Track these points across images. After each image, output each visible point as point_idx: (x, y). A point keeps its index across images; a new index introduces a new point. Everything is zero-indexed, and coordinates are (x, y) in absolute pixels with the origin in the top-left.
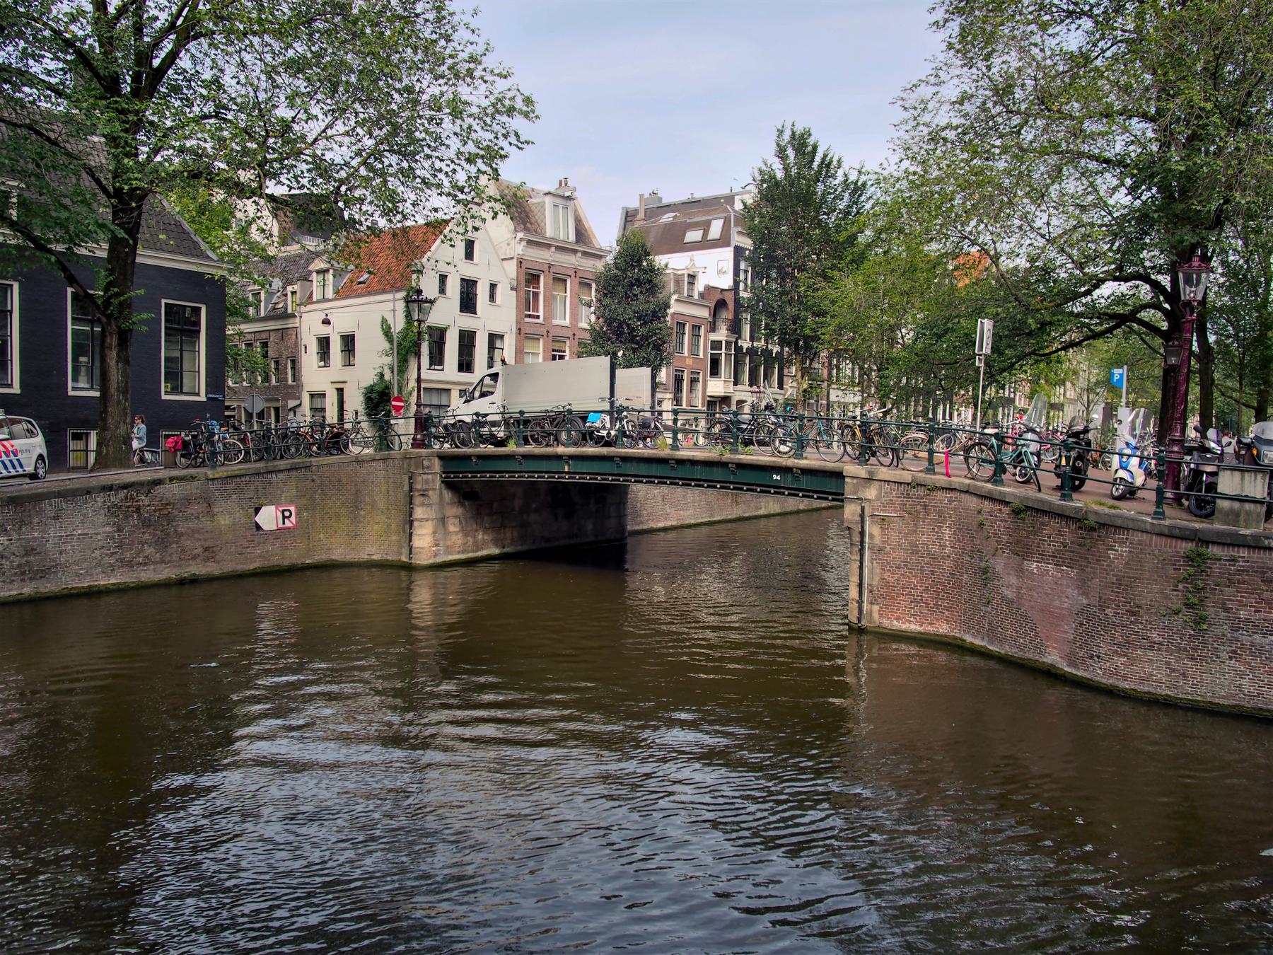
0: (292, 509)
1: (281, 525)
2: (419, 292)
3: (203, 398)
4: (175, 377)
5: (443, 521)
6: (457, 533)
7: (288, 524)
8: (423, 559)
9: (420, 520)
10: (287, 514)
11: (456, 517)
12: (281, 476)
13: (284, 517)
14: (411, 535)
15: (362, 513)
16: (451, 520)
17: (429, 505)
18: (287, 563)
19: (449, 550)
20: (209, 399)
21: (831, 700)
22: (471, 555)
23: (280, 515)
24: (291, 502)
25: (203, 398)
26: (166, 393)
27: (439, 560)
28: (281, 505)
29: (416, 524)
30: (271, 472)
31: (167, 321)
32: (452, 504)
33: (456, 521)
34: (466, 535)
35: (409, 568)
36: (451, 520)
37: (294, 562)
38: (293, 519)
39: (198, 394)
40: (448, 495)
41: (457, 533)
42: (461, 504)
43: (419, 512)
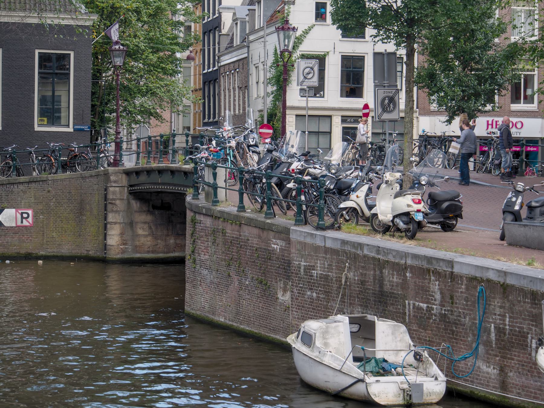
0: (30, 212)
1: (19, 223)
2: (287, 22)
3: (71, 129)
4: (51, 113)
5: (131, 224)
6: (146, 236)
7: (25, 223)
8: (114, 254)
9: (111, 223)
10: (25, 215)
11: (145, 223)
12: (21, 187)
13: (22, 218)
14: (105, 235)
15: (84, 218)
16: (140, 225)
17: (117, 212)
18: (23, 251)
19: (136, 249)
20: (75, 130)
21: (91, 319)
22: (161, 255)
23: (19, 216)
24: (29, 207)
25: (71, 129)
26: (39, 125)
27: (126, 256)
28: (21, 208)
29: (108, 226)
30: (13, 184)
31: (40, 67)
32: (140, 211)
33: (146, 226)
34: (156, 238)
35: (103, 261)
36: (140, 225)
37: (30, 251)
38: (30, 219)
39: (68, 126)
40: (135, 205)
41: (146, 236)
42: (149, 212)
43: (111, 217)
